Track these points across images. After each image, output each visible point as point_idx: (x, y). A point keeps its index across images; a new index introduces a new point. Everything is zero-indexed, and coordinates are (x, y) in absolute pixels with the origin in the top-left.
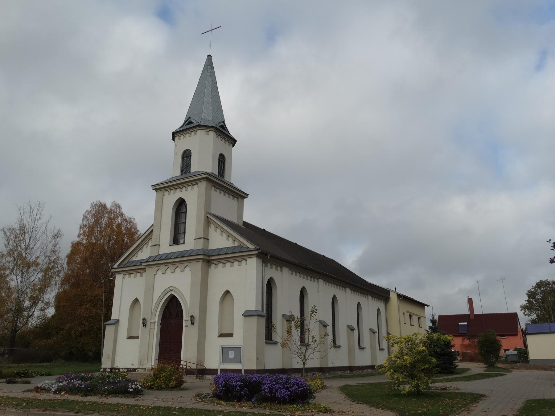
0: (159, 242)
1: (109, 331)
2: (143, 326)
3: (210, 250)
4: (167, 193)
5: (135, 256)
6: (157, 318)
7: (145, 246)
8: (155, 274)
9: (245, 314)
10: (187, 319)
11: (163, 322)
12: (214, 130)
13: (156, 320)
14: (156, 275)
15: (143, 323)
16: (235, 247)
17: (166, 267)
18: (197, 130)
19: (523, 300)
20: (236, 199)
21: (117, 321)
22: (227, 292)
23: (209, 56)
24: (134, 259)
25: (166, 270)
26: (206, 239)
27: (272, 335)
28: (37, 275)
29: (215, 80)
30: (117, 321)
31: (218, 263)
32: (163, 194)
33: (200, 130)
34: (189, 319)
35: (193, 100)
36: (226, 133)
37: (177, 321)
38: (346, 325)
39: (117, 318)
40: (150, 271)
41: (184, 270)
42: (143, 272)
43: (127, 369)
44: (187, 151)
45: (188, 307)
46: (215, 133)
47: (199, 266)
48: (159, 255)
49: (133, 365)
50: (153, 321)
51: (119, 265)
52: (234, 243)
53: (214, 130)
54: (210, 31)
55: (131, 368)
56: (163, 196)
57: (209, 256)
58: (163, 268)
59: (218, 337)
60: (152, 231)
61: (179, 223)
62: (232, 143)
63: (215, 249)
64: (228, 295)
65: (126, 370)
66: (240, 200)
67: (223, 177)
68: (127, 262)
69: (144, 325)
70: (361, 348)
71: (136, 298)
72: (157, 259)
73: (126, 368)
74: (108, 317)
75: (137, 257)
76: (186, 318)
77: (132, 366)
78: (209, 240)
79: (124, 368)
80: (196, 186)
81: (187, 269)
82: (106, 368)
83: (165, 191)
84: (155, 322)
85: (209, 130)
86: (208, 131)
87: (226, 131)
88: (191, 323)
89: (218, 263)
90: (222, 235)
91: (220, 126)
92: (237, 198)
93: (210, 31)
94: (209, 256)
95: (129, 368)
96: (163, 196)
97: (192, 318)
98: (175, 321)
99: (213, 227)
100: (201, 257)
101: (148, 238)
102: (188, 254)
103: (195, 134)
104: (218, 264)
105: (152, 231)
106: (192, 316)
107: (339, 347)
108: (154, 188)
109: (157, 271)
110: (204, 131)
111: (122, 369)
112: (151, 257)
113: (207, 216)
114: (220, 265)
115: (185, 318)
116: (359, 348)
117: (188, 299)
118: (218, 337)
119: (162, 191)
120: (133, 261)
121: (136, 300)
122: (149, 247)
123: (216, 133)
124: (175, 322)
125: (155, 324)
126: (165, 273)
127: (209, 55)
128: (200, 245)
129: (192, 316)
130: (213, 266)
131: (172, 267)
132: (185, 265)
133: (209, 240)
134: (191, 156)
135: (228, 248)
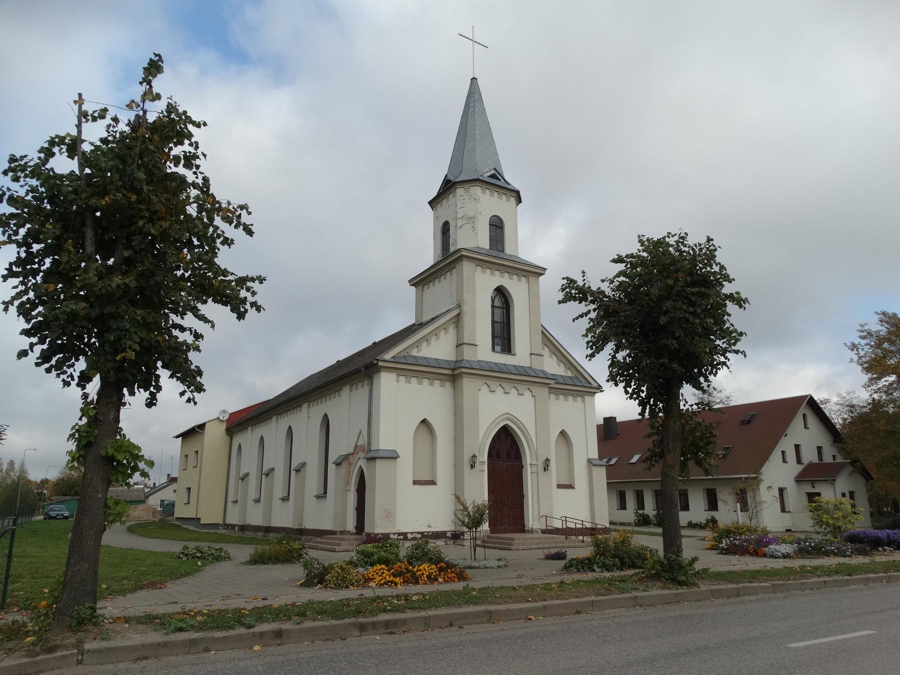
6: (484, 457)
12: (515, 196)
19: (9, 213)
20: (523, 279)
23: (474, 79)
27: (782, 439)
29: (483, 111)
36: (502, 183)
37: (510, 463)
43: (422, 533)
49: (429, 526)
53: (515, 196)
55: (429, 532)
65: (420, 536)
66: (532, 279)
67: (502, 250)
73: (418, 533)
77: (429, 528)
79: (415, 533)
82: (390, 534)
87: (500, 180)
91: (490, 176)
95: (426, 532)
96: (422, 292)
98: (506, 463)
108: (412, 283)
111: (412, 533)
127: (474, 78)
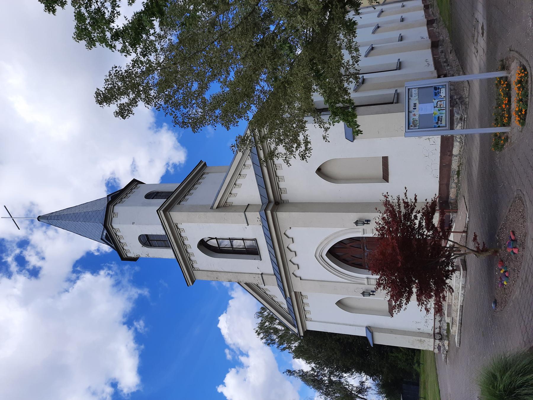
0: (259, 274)
1: (381, 339)
2: (373, 295)
3: (262, 203)
4: (195, 265)
5: (282, 305)
7: (267, 292)
8: (301, 279)
9: (351, 139)
10: (361, 230)
11: (367, 267)
13: (365, 276)
14: (302, 278)
15: (370, 295)
16: (253, 163)
17: (290, 264)
18: (113, 228)
20: (204, 176)
21: (368, 328)
22: (319, 171)
24: (285, 306)
25: (294, 264)
26: (247, 208)
28: (464, 199)
30: (368, 328)
31: (279, 188)
32: (198, 270)
33: (112, 225)
34: (361, 227)
35: (81, 234)
38: (373, 35)
39: (364, 329)
40: (298, 286)
41: (291, 238)
42: (301, 295)
44: (141, 240)
45: (342, 231)
46: (117, 204)
47: (282, 216)
48: (275, 274)
50: (365, 281)
51: (294, 326)
52: (249, 167)
53: (112, 206)
54: (13, 219)
56: (199, 270)
57: (270, 202)
58: (292, 268)
59: (388, 182)
60: (246, 284)
61: (232, 248)
62: (137, 184)
63: (261, 195)
64: (324, 170)
68: (290, 316)
69: (372, 293)
70: (400, 66)
71: (336, 304)
72: (279, 276)
74: (364, 339)
75: (282, 303)
76: (359, 232)
78: (249, 204)
80: (180, 226)
81: (289, 233)
83: (193, 267)
84: (368, 278)
85: (113, 212)
86: (113, 213)
88: (367, 224)
89: (279, 188)
90: (240, 186)
92: (203, 174)
93: (13, 219)
94: (270, 202)
96: (199, 270)
97: (359, 222)
99: (231, 200)
100: (269, 212)
101: (256, 288)
102: (268, 233)
103: (119, 230)
104: (280, 189)
105: (246, 284)
106: (357, 223)
107: (400, 63)
109: (296, 276)
110: (113, 218)
112: (278, 285)
113: (216, 208)
114: (282, 185)
115: (360, 235)
116: (399, 69)
117: (329, 231)
118: (388, 182)
119: (193, 271)
120: (288, 307)
121: (340, 303)
122: (266, 287)
123: (116, 204)
124: (367, 249)
125: (370, 279)
126: (298, 265)
128: (254, 216)
129: (357, 223)
130: (284, 197)
131: (289, 256)
132: (284, 237)
133: (249, 204)
134: (146, 235)
135: (256, 174)
